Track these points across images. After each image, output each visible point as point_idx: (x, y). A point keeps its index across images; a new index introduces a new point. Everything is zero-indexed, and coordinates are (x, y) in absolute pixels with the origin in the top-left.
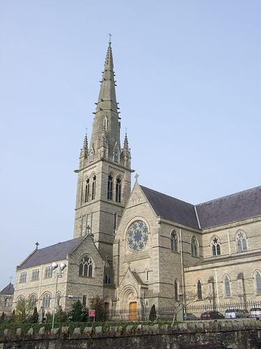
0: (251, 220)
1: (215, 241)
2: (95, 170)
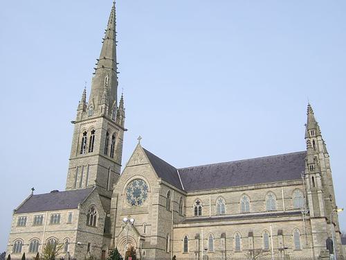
0: (231, 189)
1: (198, 203)
2: (94, 124)
